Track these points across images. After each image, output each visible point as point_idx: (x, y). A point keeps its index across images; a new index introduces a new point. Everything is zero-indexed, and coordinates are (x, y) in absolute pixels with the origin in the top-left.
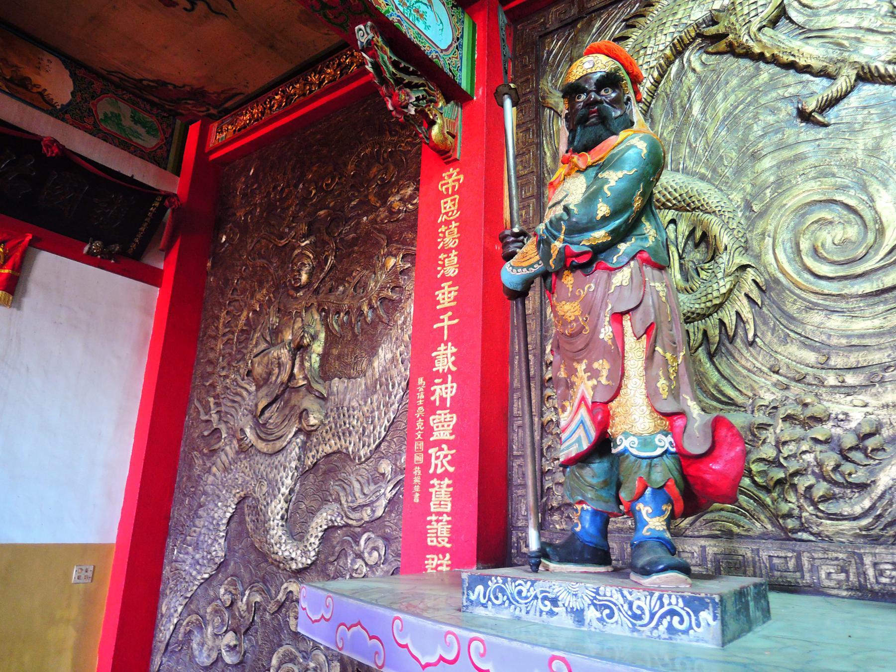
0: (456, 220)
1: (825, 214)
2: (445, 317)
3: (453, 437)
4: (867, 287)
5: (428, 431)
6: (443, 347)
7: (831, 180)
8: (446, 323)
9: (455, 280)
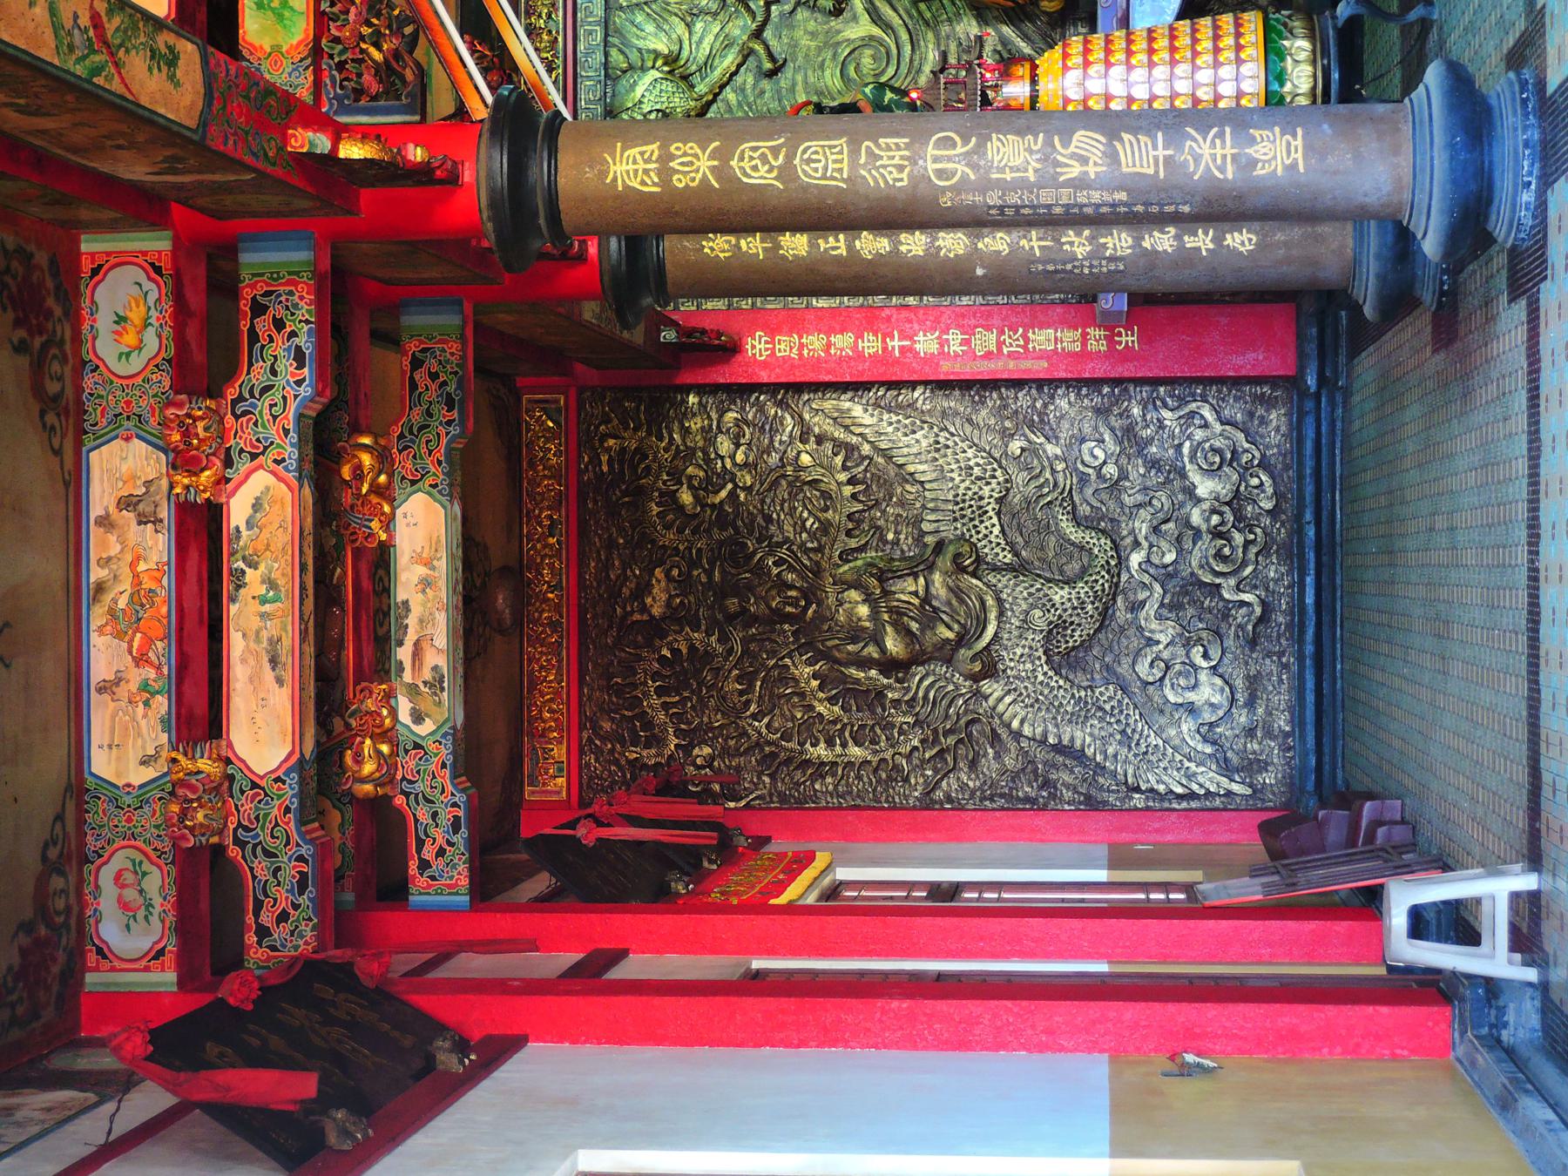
0: (801, 337)
1: (851, 69)
2: (890, 344)
3: (1299, 131)
4: (907, 49)
5: (988, 355)
6: (917, 346)
7: (827, 63)
8: (1035, 244)
9: (859, 336)
